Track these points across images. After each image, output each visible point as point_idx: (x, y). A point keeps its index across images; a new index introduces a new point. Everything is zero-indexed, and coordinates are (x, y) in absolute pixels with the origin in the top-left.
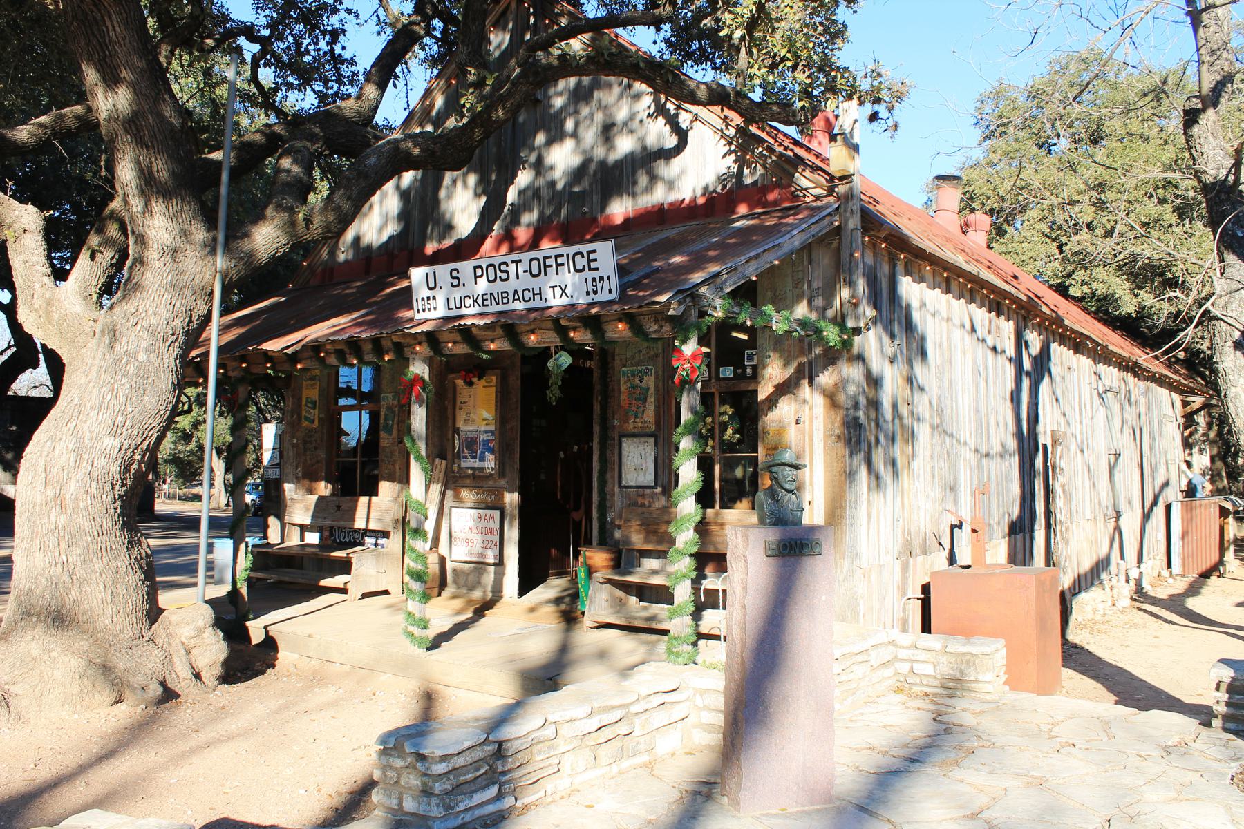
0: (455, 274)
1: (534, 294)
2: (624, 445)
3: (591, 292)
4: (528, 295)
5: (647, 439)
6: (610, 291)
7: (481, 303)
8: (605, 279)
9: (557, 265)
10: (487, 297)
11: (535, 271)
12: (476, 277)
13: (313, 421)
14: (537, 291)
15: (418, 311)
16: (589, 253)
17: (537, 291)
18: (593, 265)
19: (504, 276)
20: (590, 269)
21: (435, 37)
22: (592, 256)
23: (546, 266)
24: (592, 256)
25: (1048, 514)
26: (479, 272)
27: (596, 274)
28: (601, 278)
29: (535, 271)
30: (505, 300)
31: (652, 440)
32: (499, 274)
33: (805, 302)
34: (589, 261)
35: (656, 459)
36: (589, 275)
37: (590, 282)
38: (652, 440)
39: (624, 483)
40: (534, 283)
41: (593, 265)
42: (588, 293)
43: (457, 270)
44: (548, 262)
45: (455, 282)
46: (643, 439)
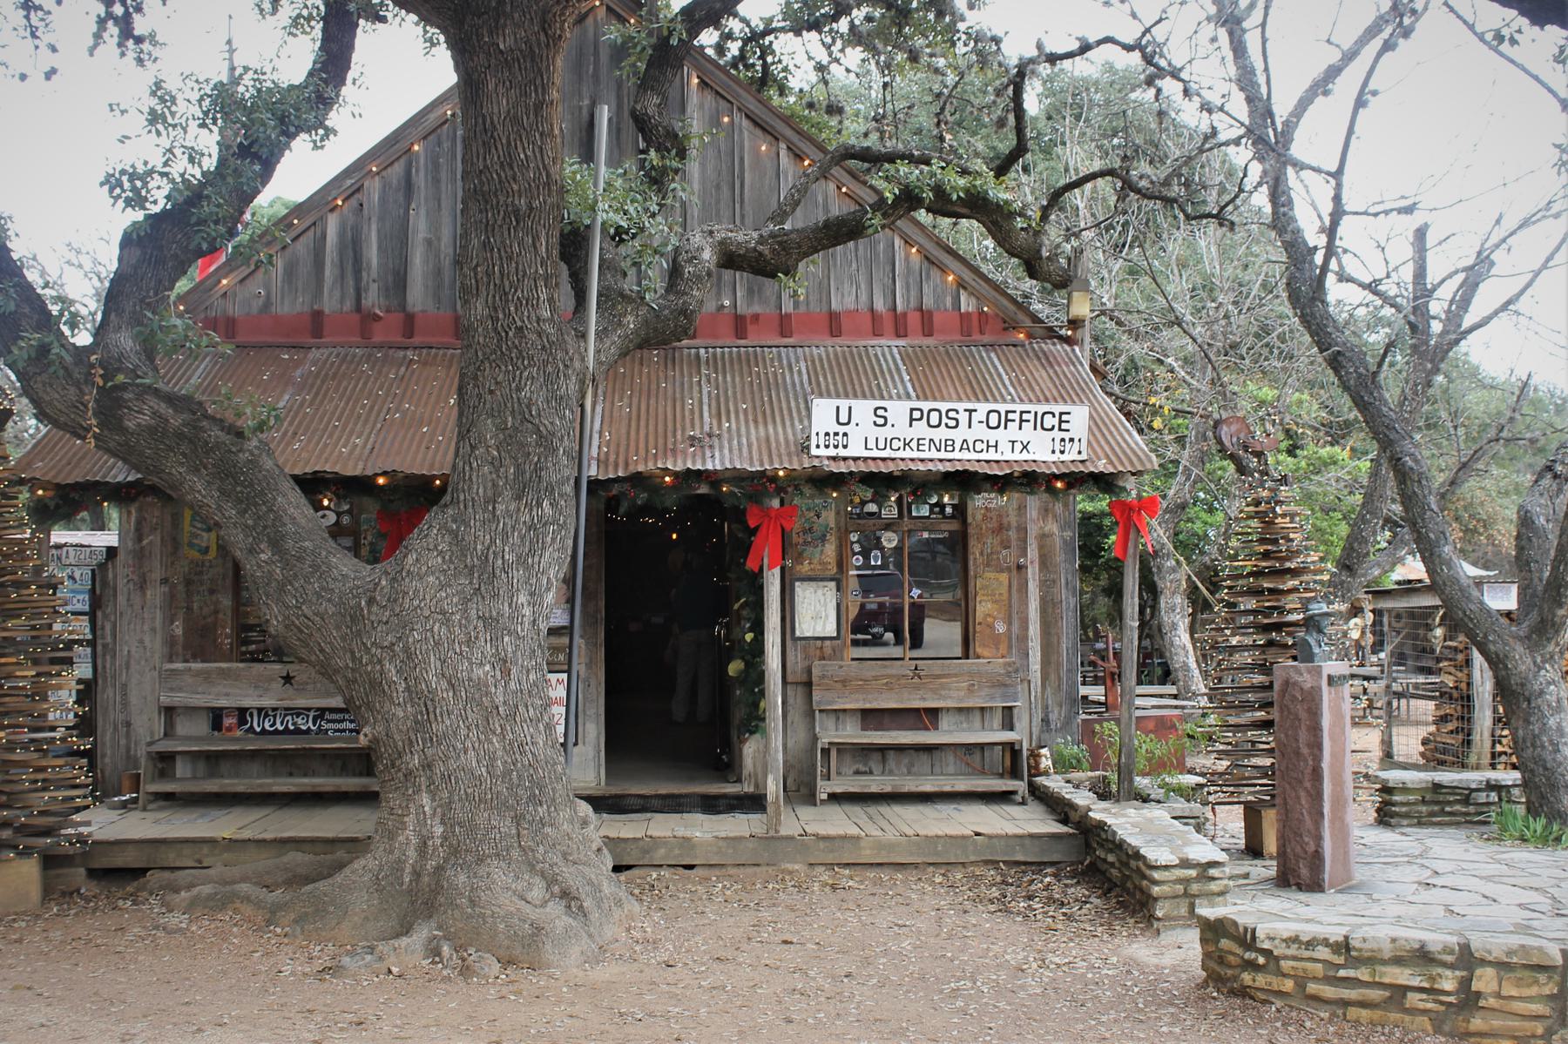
0: (880, 412)
1: (988, 446)
2: (797, 589)
3: (1057, 452)
4: (979, 446)
5: (826, 583)
6: (1080, 452)
7: (915, 448)
8: (1076, 440)
9: (1022, 421)
10: (927, 442)
11: (993, 422)
12: (912, 420)
13: (206, 550)
14: (992, 443)
15: (818, 446)
16: (1061, 414)
17: (992, 443)
18: (1064, 426)
19: (952, 423)
20: (1060, 429)
21: (782, 30)
22: (1064, 417)
23: (1007, 421)
24: (1064, 417)
25: (883, 750)
26: (916, 415)
27: (1067, 436)
28: (1072, 440)
29: (993, 422)
30: (949, 448)
31: (833, 584)
32: (945, 420)
33: (704, 310)
34: (1061, 422)
35: (838, 606)
36: (1058, 435)
37: (1057, 441)
38: (833, 584)
39: (798, 634)
40: (992, 436)
41: (1064, 426)
42: (1053, 452)
43: (886, 410)
44: (1010, 416)
45: (881, 421)
46: (821, 584)
